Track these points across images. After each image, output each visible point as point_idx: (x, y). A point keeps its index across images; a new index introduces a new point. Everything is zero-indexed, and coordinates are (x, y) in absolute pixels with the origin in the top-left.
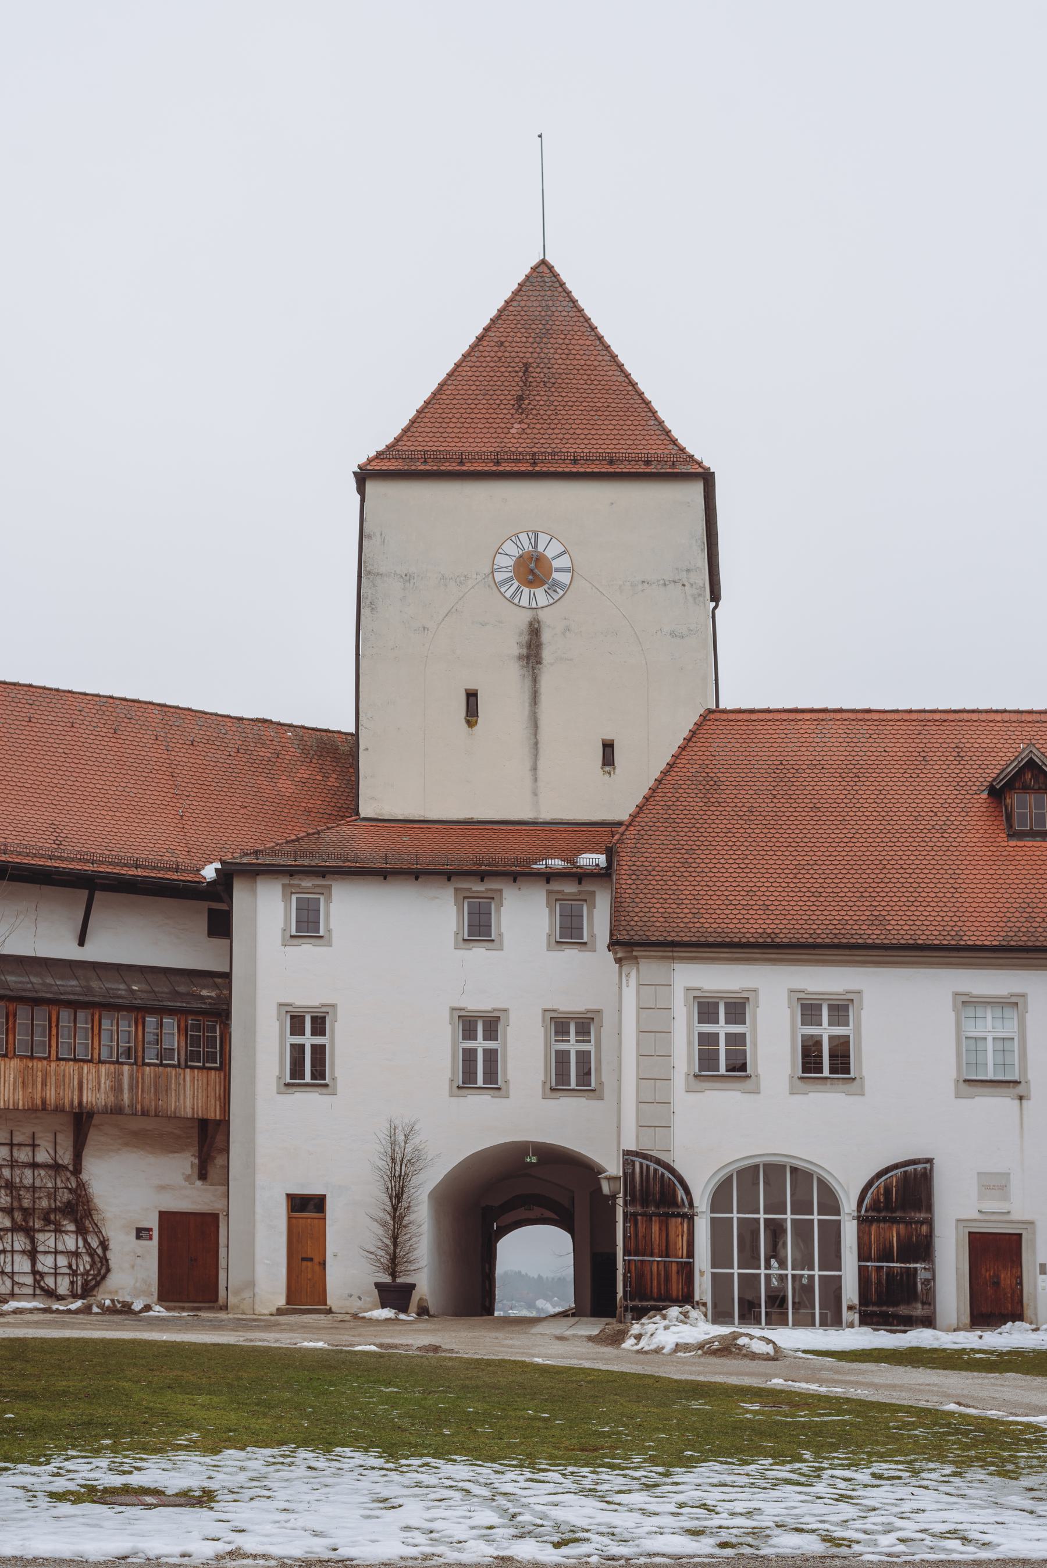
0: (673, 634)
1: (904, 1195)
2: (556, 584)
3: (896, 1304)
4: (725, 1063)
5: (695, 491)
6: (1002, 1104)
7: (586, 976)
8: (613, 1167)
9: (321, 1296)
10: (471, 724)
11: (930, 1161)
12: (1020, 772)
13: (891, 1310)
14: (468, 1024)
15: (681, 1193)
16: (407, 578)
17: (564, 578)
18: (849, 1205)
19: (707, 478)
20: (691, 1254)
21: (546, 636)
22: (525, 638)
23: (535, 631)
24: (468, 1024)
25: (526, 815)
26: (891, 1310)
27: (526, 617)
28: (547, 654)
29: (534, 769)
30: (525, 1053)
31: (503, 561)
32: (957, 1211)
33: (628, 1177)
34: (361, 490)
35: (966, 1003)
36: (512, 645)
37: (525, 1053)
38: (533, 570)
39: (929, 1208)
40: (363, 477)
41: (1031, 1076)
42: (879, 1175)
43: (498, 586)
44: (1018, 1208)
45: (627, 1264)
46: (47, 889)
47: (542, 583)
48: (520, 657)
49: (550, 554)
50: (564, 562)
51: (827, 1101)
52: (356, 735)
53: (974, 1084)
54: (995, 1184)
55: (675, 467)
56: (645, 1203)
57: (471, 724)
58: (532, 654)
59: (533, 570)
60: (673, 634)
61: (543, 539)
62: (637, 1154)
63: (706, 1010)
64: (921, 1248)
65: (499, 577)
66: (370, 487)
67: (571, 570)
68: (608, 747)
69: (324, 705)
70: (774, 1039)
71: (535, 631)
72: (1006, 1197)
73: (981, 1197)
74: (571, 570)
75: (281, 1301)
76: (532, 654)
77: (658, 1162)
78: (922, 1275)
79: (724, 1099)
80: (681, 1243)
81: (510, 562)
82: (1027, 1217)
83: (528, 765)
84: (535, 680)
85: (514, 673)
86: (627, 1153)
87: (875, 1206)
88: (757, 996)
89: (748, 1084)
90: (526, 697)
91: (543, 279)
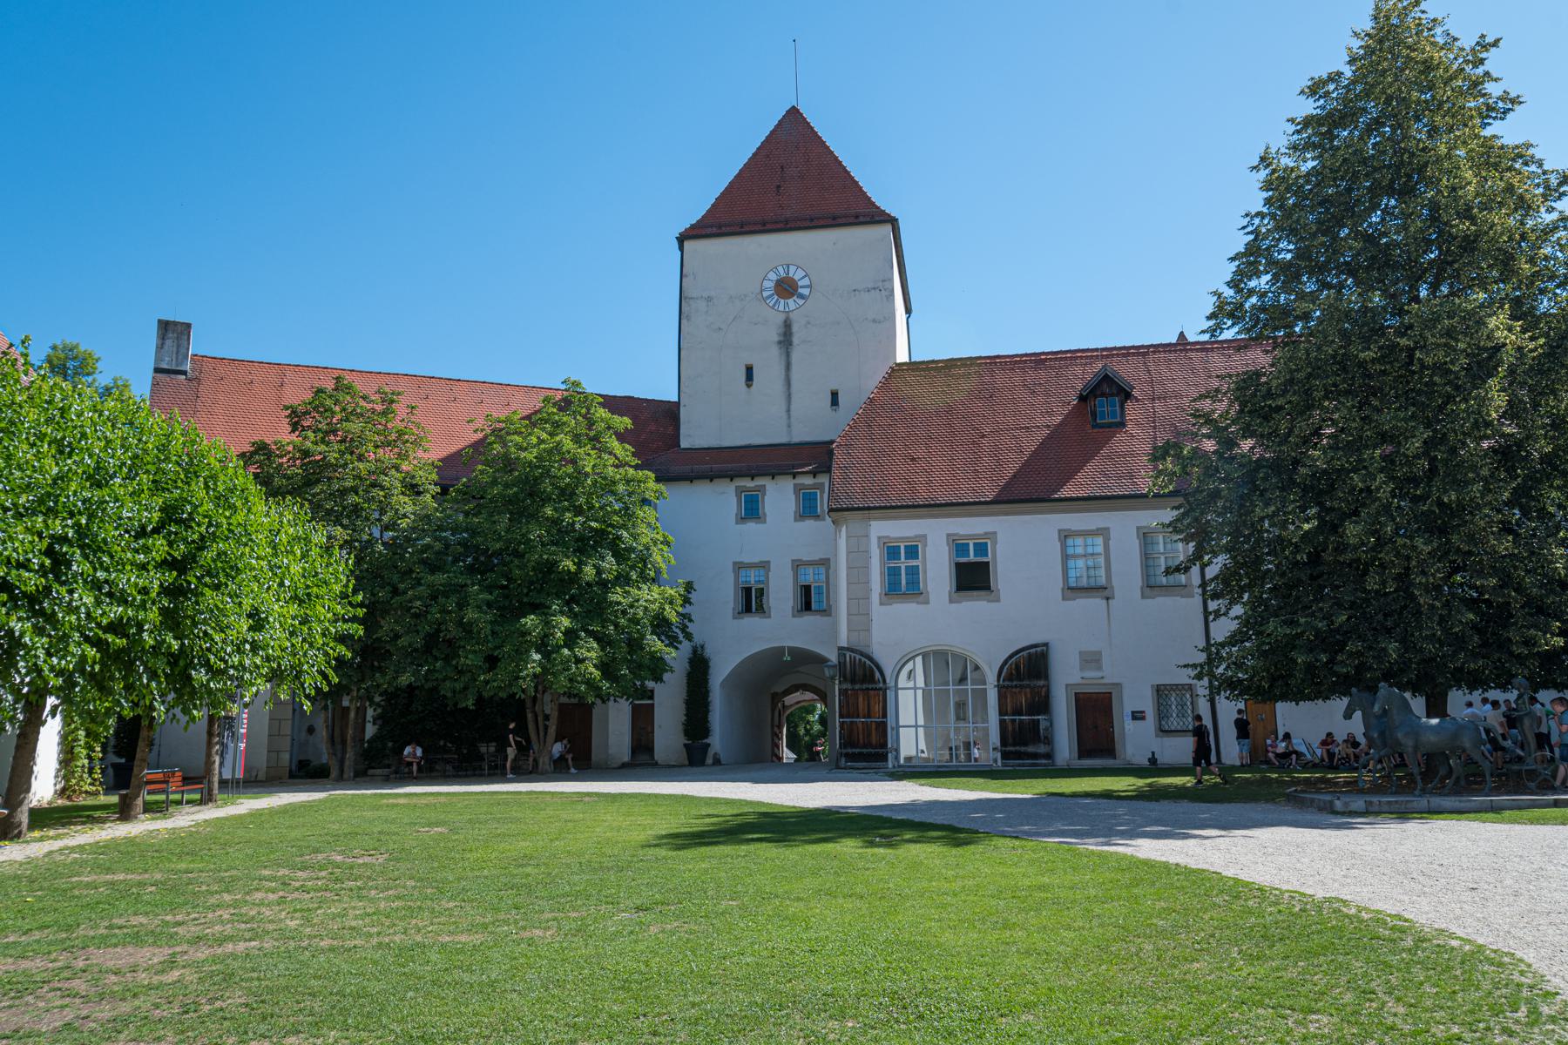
0: (874, 321)
1: (1028, 671)
2: (802, 296)
3: (1026, 745)
4: (903, 584)
5: (889, 227)
6: (1095, 603)
7: (808, 538)
8: (833, 657)
9: (650, 749)
10: (749, 386)
11: (1046, 645)
12: (1099, 384)
13: (1023, 749)
14: (165, 327)
15: (877, 675)
16: (709, 299)
17: (805, 292)
18: (991, 678)
19: (893, 222)
20: (885, 715)
21: (795, 328)
22: (782, 330)
23: (787, 326)
24: (165, 327)
25: (784, 440)
26: (1023, 749)
27: (782, 317)
28: (795, 340)
29: (788, 410)
30: (781, 594)
31: (768, 284)
32: (1066, 677)
33: (842, 665)
34: (681, 248)
35: (1065, 536)
36: (774, 335)
37: (781, 594)
38: (786, 288)
39: (1047, 677)
40: (681, 239)
41: (1115, 582)
42: (1011, 657)
43: (765, 299)
44: (1109, 674)
45: (842, 724)
46: (975, 593)
47: (792, 295)
48: (780, 342)
49: (796, 278)
50: (806, 282)
51: (975, 606)
52: (678, 404)
53: (1073, 591)
54: (1091, 660)
55: (875, 216)
56: (853, 681)
57: (749, 386)
58: (786, 339)
59: (786, 288)
60: (874, 321)
61: (792, 269)
62: (848, 649)
63: (892, 553)
64: (1042, 704)
65: (765, 294)
66: (686, 244)
67: (810, 286)
68: (835, 395)
69: (656, 382)
70: (938, 571)
71: (787, 326)
72: (1100, 668)
73: (1082, 669)
74: (810, 286)
75: (626, 758)
76: (786, 339)
77: (862, 654)
78: (1043, 725)
79: (905, 610)
80: (877, 708)
81: (772, 284)
82: (1116, 681)
83: (784, 408)
84: (788, 355)
85: (775, 352)
86: (841, 649)
87: (1009, 678)
88: (995, 543)
89: (921, 598)
90: (783, 367)
91: (794, 112)
